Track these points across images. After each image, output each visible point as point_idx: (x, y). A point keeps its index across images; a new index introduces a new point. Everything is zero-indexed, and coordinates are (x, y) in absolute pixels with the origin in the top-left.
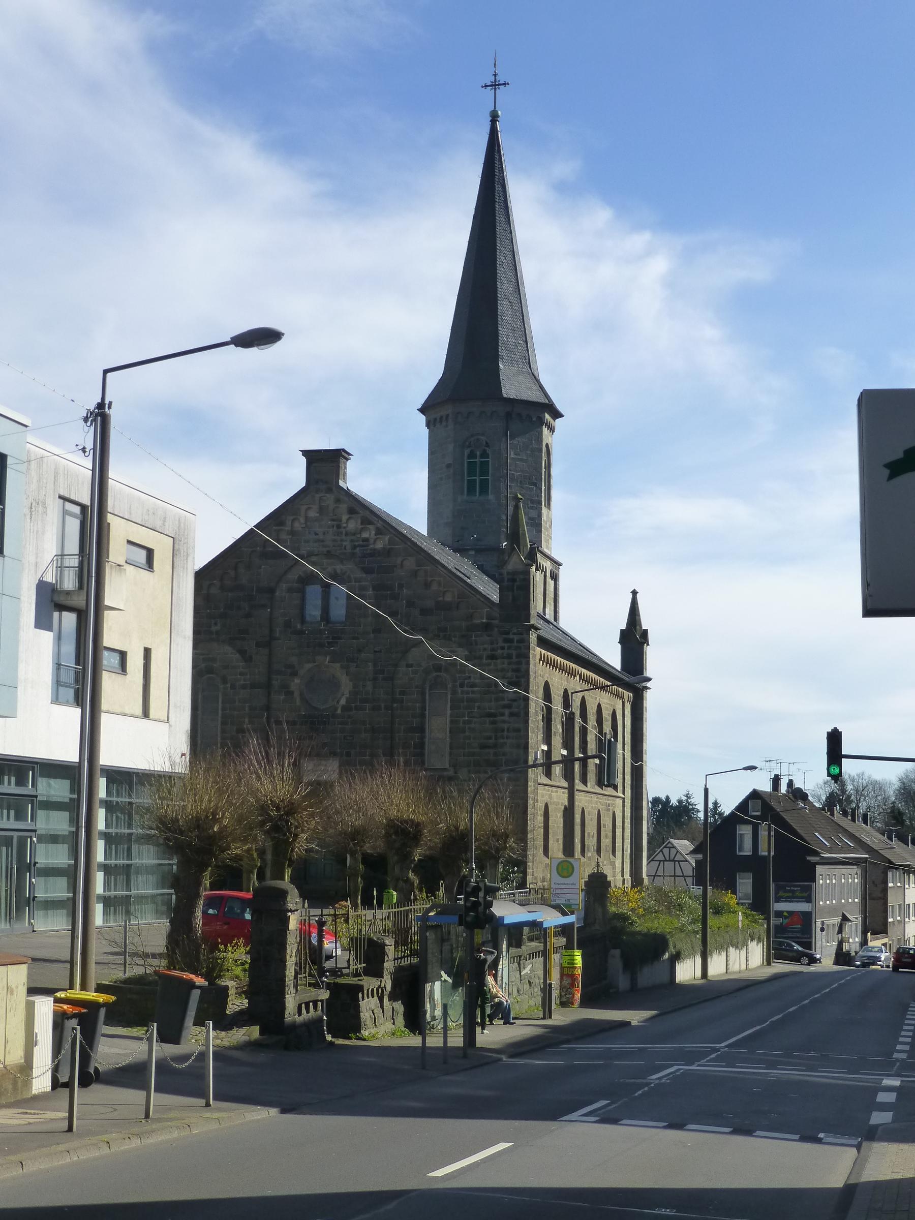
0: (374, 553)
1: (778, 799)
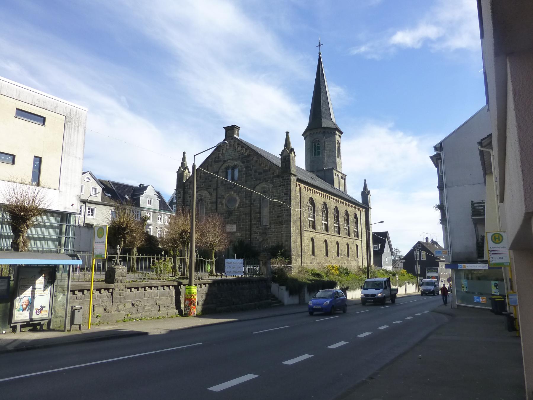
0: (245, 157)
1: (427, 244)
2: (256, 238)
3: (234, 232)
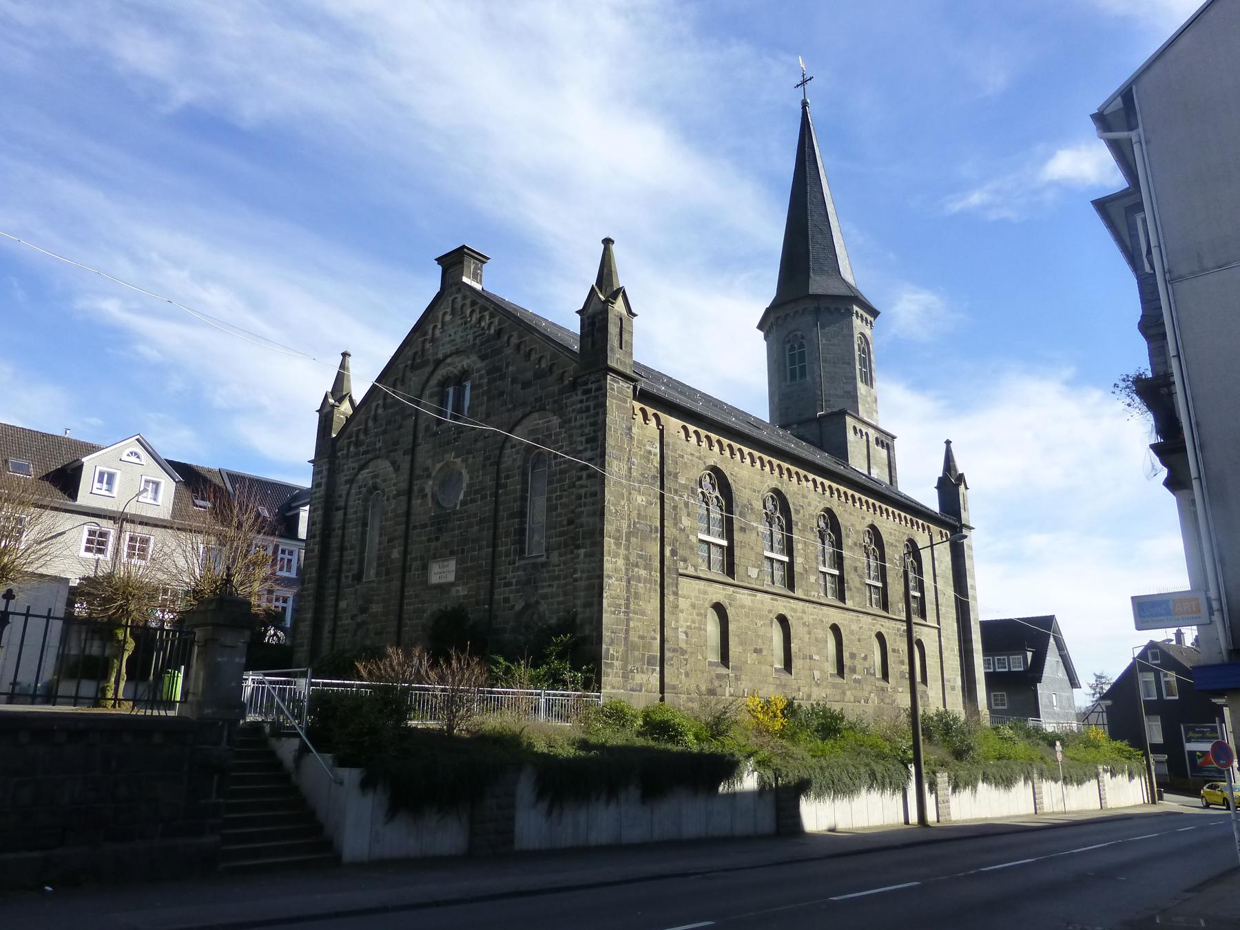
2: (506, 600)
3: (452, 584)
